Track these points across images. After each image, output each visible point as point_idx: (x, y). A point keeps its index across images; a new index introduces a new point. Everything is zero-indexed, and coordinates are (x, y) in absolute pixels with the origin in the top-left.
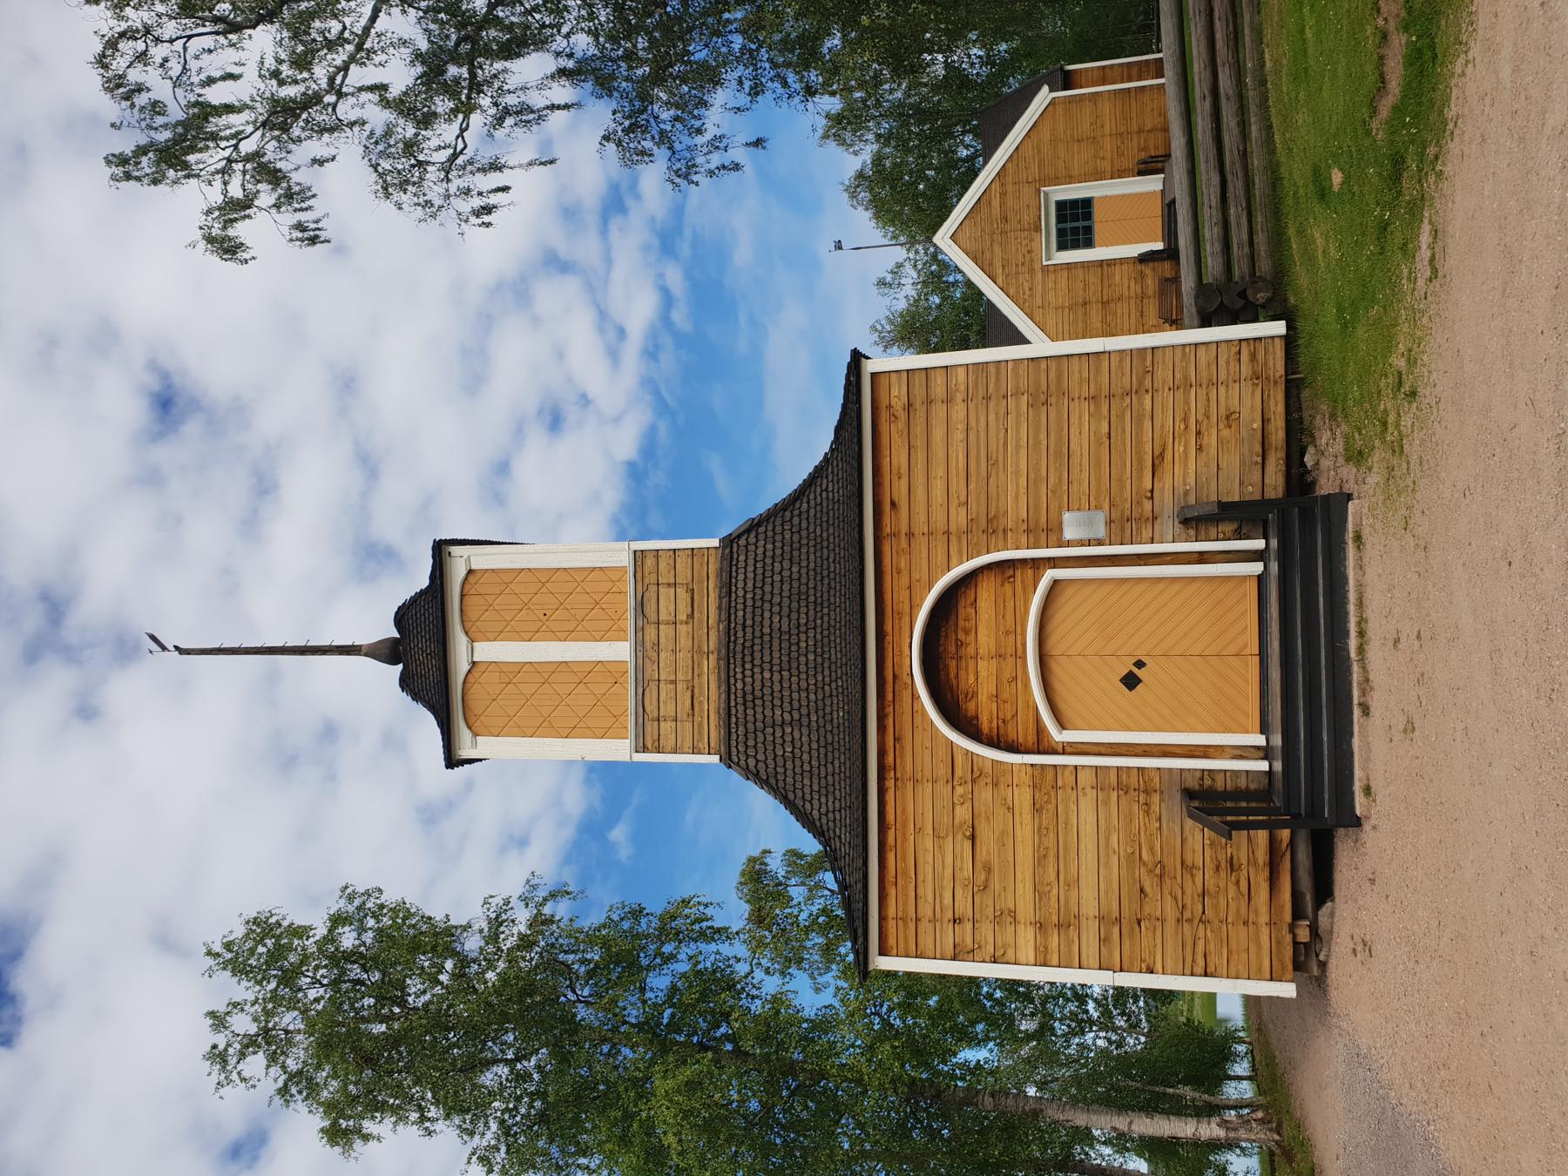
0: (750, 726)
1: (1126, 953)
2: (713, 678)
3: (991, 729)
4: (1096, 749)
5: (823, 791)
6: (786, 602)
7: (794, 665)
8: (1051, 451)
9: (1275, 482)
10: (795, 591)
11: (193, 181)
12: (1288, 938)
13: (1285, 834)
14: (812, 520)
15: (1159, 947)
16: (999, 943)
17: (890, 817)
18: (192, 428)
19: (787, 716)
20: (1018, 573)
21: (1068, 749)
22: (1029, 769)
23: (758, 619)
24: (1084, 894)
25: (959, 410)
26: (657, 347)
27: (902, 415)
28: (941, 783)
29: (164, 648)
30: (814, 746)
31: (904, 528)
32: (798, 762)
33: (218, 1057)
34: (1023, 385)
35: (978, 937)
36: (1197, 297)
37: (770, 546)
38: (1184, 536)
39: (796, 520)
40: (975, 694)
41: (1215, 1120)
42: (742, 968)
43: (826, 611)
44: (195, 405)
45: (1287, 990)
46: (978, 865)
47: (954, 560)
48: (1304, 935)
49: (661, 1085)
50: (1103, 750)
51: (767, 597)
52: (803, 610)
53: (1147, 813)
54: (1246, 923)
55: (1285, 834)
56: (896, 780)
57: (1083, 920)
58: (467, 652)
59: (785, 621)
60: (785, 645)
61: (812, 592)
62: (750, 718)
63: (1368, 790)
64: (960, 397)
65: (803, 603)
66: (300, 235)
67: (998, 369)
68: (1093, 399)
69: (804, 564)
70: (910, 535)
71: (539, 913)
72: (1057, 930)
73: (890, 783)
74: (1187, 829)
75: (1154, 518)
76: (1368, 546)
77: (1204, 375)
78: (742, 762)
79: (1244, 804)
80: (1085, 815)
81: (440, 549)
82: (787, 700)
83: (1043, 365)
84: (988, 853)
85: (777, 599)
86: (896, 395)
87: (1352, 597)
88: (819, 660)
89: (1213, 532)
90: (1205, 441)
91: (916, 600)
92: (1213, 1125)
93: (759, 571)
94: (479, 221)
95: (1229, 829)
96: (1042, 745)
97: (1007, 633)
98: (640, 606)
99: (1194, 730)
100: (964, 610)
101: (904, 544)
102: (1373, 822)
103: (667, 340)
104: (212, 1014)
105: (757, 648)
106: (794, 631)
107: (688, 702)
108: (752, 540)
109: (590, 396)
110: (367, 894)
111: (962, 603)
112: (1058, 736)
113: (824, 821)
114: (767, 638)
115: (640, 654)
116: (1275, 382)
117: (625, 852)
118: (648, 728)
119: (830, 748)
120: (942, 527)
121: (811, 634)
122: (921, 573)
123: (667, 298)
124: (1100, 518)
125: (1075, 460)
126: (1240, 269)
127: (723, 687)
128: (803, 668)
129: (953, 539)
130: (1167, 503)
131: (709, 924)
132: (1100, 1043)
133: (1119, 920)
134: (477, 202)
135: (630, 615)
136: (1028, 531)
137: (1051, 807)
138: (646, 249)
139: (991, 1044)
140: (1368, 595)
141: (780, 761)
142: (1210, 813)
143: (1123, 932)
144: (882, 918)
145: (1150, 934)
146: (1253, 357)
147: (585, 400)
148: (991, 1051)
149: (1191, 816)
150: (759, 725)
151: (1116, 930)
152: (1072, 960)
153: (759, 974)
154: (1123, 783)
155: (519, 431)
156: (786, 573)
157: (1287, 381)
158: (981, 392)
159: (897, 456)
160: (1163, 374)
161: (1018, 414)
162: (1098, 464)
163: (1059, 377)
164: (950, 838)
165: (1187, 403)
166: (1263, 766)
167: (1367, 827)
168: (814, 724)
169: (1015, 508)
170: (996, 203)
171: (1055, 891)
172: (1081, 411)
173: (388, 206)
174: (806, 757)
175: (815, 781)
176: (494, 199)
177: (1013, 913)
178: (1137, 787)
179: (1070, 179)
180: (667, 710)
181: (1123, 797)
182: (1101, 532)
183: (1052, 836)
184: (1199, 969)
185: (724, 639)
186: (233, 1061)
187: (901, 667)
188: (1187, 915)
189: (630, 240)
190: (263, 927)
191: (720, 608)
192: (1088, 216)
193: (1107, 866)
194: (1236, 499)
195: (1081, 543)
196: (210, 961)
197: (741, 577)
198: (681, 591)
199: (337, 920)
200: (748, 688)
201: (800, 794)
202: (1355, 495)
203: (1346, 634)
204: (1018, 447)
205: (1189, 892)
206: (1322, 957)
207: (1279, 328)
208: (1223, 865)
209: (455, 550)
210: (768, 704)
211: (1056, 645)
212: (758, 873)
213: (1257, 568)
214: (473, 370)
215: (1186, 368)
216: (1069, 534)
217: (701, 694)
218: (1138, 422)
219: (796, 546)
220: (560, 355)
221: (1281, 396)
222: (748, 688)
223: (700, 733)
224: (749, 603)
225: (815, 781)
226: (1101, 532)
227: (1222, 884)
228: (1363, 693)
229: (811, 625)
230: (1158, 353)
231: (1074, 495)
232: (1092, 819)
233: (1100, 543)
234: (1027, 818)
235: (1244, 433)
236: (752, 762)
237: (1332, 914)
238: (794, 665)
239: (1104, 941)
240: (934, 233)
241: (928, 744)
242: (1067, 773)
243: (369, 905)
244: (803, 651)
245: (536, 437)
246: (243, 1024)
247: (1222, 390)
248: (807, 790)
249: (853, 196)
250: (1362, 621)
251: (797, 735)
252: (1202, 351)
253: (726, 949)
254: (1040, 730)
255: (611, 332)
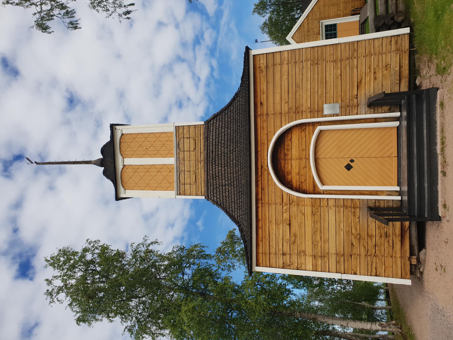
0: (215, 186)
1: (346, 267)
2: (202, 170)
3: (296, 185)
4: (335, 192)
5: (238, 208)
6: (226, 142)
7: (229, 165)
8: (319, 81)
9: (404, 88)
10: (229, 139)
11: (33, 6)
12: (408, 263)
13: (407, 223)
14: (234, 113)
15: (359, 265)
16: (299, 263)
17: (260, 217)
18: (78, 108)
19: (226, 182)
20: (307, 128)
21: (325, 192)
22: (310, 200)
23: (217, 149)
24: (330, 245)
25: (285, 67)
26: (209, 83)
27: (264, 70)
28: (278, 205)
29: (32, 163)
30: (236, 192)
31: (265, 112)
32: (230, 198)
33: (50, 294)
34: (309, 58)
35: (291, 260)
36: (374, 21)
37: (221, 123)
38: (369, 112)
39: (229, 113)
40: (291, 173)
41: (378, 323)
42: (214, 269)
43: (239, 145)
44: (79, 101)
45: (408, 282)
46: (292, 234)
47: (283, 123)
48: (414, 262)
49: (184, 308)
50: (338, 193)
51: (220, 141)
52: (232, 145)
53: (354, 216)
54: (392, 257)
55: (407, 223)
56: (262, 204)
57: (330, 255)
58: (121, 162)
59: (226, 149)
60: (226, 158)
61: (234, 138)
62: (215, 183)
63: (445, 206)
64: (285, 62)
65: (232, 143)
66: (71, 26)
67: (299, 52)
68: (335, 61)
69: (232, 129)
70: (267, 115)
71: (147, 249)
72: (320, 257)
73: (260, 205)
74: (369, 222)
75: (358, 105)
76: (447, 107)
77: (377, 50)
78: (212, 199)
79: (391, 212)
80: (331, 217)
81: (113, 127)
82: (226, 177)
83: (316, 49)
84: (295, 230)
85: (223, 142)
86: (262, 62)
87: (438, 129)
88: (237, 162)
89: (380, 110)
90: (377, 76)
91: (269, 139)
92: (377, 325)
93: (217, 132)
94: (126, 17)
95: (387, 222)
96: (315, 191)
97: (303, 150)
98: (178, 145)
99: (372, 185)
100: (287, 142)
101: (265, 118)
102: (447, 218)
103: (212, 81)
104: (47, 280)
105: (217, 159)
106: (229, 153)
107: (194, 178)
108: (215, 121)
109: (191, 98)
110: (95, 241)
111: (286, 140)
112: (321, 188)
113: (239, 219)
114: (220, 156)
115: (178, 162)
116: (405, 52)
117: (201, 228)
118: (181, 187)
119: (240, 193)
120: (279, 111)
121: (234, 153)
122: (271, 129)
123: (212, 67)
124: (337, 106)
125: (328, 85)
126: (392, 9)
127: (206, 173)
128: (232, 165)
129: (283, 116)
130: (363, 100)
131: (204, 253)
132: (338, 288)
133: (344, 255)
134: (124, 10)
135: (175, 149)
136: (311, 112)
137: (319, 213)
138: (206, 54)
139: (305, 288)
140: (446, 127)
141: (224, 198)
142: (379, 215)
143: (345, 259)
144: (257, 253)
145: (355, 260)
146: (396, 42)
147: (189, 99)
148: (305, 290)
149: (371, 216)
150: (218, 186)
151: (342, 259)
152: (326, 269)
153: (220, 271)
154: (345, 205)
155: (170, 108)
156: (226, 133)
157: (410, 51)
158: (293, 60)
159: (263, 86)
160: (361, 51)
161: (307, 68)
162: (337, 86)
163: (322, 54)
164: (282, 225)
165: (370, 61)
166: (399, 198)
167: (444, 221)
168: (235, 185)
169: (306, 103)
170: (306, 26)
171: (320, 244)
172: (330, 66)
173: (94, 11)
174: (233, 196)
175: (236, 205)
176: (130, 8)
177: (304, 252)
178: (351, 206)
179: (329, 18)
180: (187, 181)
181: (345, 210)
182: (338, 111)
183: (319, 224)
184: (374, 273)
185: (206, 156)
186: (55, 295)
187: (264, 163)
188: (369, 253)
189: (201, 52)
190: (64, 252)
191: (204, 146)
192: (335, 29)
193: (339, 235)
194: (389, 92)
195: (330, 116)
196: (46, 263)
197: (211, 134)
198: (191, 140)
199: (85, 250)
200: (214, 173)
201: (231, 209)
202: (441, 87)
203: (436, 144)
204: (307, 80)
205: (370, 245)
206: (421, 270)
207: (407, 30)
208: (383, 235)
209: (117, 127)
210: (220, 178)
211: (321, 154)
212: (232, 236)
213: (397, 124)
214: (157, 91)
215: (370, 48)
216: (326, 112)
217: (198, 175)
218: (352, 69)
219: (229, 122)
220: (181, 86)
221: (407, 57)
222: (214, 173)
223: (198, 189)
224: (214, 143)
225: (236, 205)
226: (338, 111)
227: (383, 242)
228: (443, 167)
229: (234, 150)
230: (359, 43)
231: (328, 98)
232: (333, 218)
233: (337, 115)
234: (310, 218)
235: (392, 72)
236: (215, 198)
237: (425, 254)
238: (229, 165)
239: (338, 262)
240: (287, 36)
241: (274, 191)
242: (324, 201)
243: (96, 246)
244: (232, 159)
245: (175, 110)
246: (58, 283)
247: (384, 56)
248: (233, 208)
249: (263, 30)
250: (443, 138)
251: (230, 189)
252: (376, 41)
253: (210, 262)
254: (315, 185)
255: (196, 79)
